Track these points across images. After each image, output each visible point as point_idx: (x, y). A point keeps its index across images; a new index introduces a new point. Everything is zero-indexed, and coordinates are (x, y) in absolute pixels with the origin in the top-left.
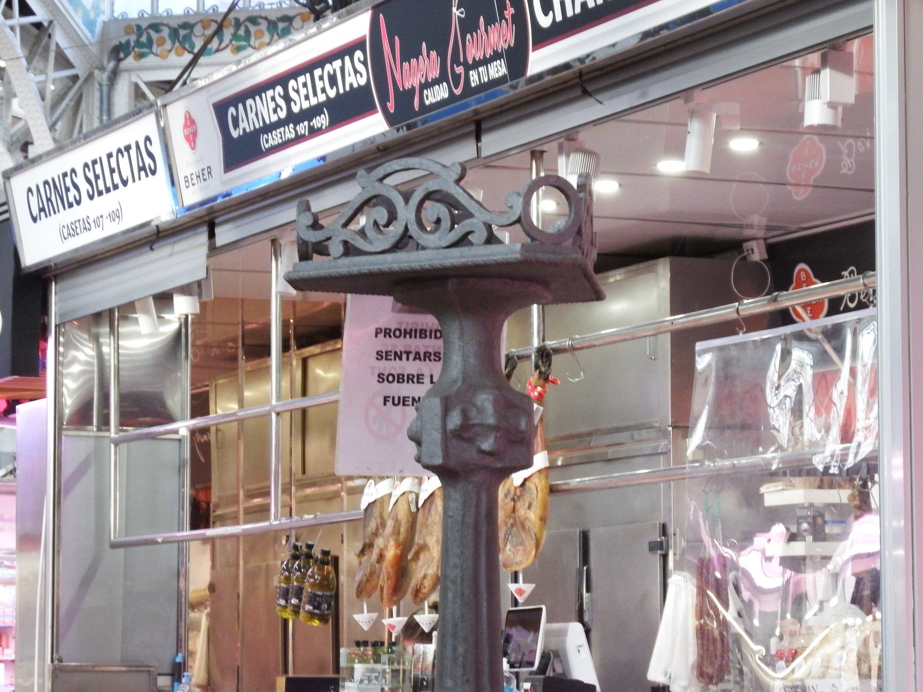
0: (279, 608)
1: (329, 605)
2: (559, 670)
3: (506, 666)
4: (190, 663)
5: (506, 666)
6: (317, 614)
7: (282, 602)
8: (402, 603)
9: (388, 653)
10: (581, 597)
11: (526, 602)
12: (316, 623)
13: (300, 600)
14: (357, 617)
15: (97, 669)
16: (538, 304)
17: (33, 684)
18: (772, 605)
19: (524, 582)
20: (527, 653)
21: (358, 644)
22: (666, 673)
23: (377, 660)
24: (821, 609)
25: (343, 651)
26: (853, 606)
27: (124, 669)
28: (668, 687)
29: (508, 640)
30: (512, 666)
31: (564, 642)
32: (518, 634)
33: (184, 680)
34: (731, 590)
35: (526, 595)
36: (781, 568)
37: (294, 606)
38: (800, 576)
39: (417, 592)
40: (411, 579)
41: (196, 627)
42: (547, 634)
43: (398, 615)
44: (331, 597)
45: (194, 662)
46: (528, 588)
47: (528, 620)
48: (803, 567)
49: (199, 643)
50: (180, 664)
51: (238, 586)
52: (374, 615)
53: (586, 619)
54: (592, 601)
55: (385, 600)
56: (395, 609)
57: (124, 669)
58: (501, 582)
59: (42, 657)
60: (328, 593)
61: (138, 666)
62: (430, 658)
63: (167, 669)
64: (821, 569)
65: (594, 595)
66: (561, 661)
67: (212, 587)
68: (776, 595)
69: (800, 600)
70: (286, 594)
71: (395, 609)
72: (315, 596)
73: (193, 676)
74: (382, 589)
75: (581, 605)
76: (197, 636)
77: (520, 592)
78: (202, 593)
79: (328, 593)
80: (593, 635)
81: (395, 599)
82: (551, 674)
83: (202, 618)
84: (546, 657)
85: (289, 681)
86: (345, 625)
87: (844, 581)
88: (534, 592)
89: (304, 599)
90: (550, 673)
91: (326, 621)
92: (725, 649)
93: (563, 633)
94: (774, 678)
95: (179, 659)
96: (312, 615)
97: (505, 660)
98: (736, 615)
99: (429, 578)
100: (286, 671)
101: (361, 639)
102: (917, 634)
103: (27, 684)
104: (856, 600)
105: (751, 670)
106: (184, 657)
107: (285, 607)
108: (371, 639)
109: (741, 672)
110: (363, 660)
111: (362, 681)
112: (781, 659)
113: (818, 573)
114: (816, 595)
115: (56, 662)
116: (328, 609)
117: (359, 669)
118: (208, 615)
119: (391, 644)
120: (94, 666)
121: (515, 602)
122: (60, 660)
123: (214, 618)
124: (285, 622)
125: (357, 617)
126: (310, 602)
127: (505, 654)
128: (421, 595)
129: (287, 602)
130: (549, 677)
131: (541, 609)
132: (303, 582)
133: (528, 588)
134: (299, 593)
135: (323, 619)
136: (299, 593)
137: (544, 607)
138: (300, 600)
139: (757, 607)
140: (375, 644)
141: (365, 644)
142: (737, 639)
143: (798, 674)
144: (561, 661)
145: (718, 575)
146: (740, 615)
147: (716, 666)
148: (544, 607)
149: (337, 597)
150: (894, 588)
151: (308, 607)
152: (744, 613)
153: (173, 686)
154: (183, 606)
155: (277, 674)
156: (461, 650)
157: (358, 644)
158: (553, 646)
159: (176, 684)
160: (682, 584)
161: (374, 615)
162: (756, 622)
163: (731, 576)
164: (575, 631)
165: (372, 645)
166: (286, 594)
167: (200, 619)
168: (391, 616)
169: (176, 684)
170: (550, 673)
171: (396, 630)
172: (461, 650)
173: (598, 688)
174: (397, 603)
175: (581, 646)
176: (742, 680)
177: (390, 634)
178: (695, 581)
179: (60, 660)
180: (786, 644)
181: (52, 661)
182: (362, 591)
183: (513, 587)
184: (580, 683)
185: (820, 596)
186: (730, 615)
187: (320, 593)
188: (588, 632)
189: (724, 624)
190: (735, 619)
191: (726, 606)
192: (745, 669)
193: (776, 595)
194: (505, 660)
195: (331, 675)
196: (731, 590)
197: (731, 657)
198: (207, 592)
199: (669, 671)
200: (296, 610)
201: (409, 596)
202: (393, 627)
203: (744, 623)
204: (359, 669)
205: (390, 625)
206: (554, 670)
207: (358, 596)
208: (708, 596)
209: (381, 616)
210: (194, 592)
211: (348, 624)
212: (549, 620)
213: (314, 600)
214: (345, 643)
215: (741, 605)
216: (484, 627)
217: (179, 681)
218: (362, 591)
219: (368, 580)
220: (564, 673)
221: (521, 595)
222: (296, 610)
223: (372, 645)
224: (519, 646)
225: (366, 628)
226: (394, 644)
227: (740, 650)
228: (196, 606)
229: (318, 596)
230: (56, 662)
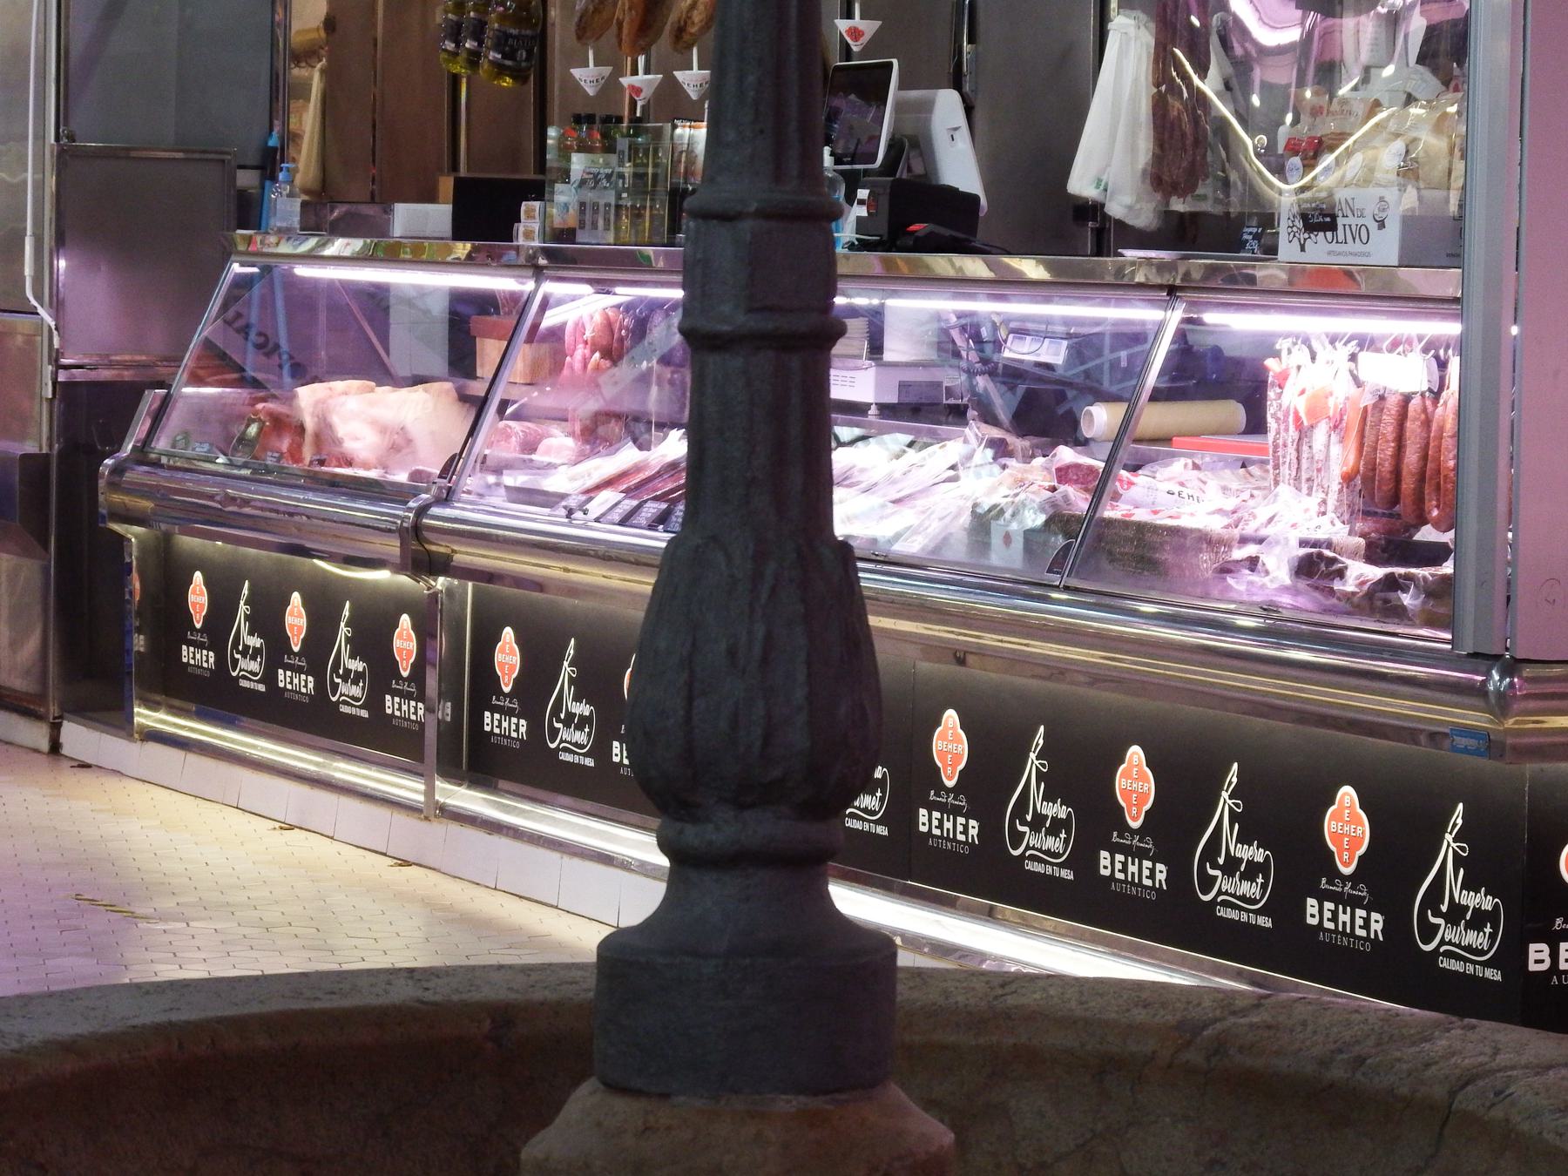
0: (443, 56)
1: (530, 52)
2: (918, 169)
3: (828, 160)
4: (292, 152)
5: (828, 160)
6: (509, 67)
7: (450, 46)
8: (654, 48)
9: (629, 135)
10: (959, 51)
11: (865, 53)
12: (507, 82)
13: (481, 44)
14: (577, 73)
15: (133, 154)
16: (832, 292)
17: (25, 182)
18: (1282, 74)
19: (862, 18)
20: (864, 140)
21: (578, 120)
22: (1099, 181)
23: (609, 148)
24: (1366, 80)
25: (552, 132)
26: (1420, 67)
27: (180, 155)
28: (1103, 205)
29: (833, 116)
30: (838, 160)
31: (928, 121)
32: (849, 105)
33: (281, 176)
34: (1214, 41)
35: (865, 39)
36: (1299, 13)
37: (470, 52)
38: (1330, 21)
39: (680, 31)
40: (669, 9)
41: (303, 91)
42: (900, 107)
43: (647, 72)
44: (533, 38)
45: (299, 152)
46: (869, 27)
47: (871, 84)
48: (1338, 8)
49: (307, 120)
50: (274, 149)
51: (375, 25)
52: (607, 70)
53: (967, 88)
54: (976, 57)
55: (625, 45)
56: (641, 60)
57: (180, 155)
58: (824, 16)
59: (40, 136)
60: (528, 32)
61: (204, 152)
62: (700, 148)
63: (253, 157)
64: (1368, 11)
65: (980, 48)
66: (921, 154)
67: (330, 24)
68: (1289, 58)
69: (1328, 72)
70: (455, 33)
71: (641, 60)
72: (507, 36)
73: (296, 170)
74: (620, 25)
75: (959, 65)
76: (305, 108)
77: (856, 33)
78: (314, 35)
79: (528, 32)
80: (978, 114)
81: (642, 43)
82: (905, 176)
83: (314, 78)
84: (895, 146)
85: (459, 183)
86: (557, 92)
87: (1406, 36)
88: (877, 35)
89: (488, 42)
90: (902, 173)
91: (525, 80)
92: (1199, 142)
93: (927, 107)
94: (1280, 193)
95: (273, 142)
96: (500, 70)
97: (827, 150)
98: (1221, 87)
99: (701, 7)
100: (455, 167)
101: (583, 111)
102: (1527, 117)
103: (15, 181)
104: (1426, 57)
105: (1244, 178)
106: (282, 138)
107: (455, 54)
108: (600, 113)
109: (1226, 184)
110: (583, 148)
111: (583, 183)
112: (1296, 154)
113: (1363, 18)
114: (1357, 59)
115: (64, 141)
116: (527, 59)
117: (579, 164)
118: (322, 71)
119: (634, 120)
120: (128, 149)
121: (847, 53)
122: (71, 138)
123: (332, 77)
124: (455, 80)
125: (577, 73)
126: (497, 47)
127: (828, 142)
128: (686, 37)
129: (458, 46)
130: (900, 180)
131: (891, 64)
132: (487, 13)
133: (869, 27)
134: (478, 32)
135: (519, 76)
136: (478, 32)
137: (895, 62)
138: (481, 44)
139: (1257, 74)
140: (607, 120)
141: (590, 119)
142: (1222, 126)
143: (1326, 182)
144: (921, 154)
145: (1195, 21)
146: (1228, 86)
147: (1185, 164)
148: (895, 62)
149: (542, 38)
150: (1492, 52)
151: (493, 55)
152: (1234, 83)
153: (263, 188)
154: (282, 54)
155: (440, 170)
156: (751, 79)
157: (578, 120)
158: (909, 129)
159: (268, 183)
160: (1132, 31)
161: (607, 70)
162: (1256, 100)
163: (1215, 20)
164: (947, 104)
165: (601, 124)
166: (455, 33)
167: (311, 78)
168: (635, 72)
169: (268, 183)
170: (902, 173)
171: (643, 95)
172: (751, 79)
173: (983, 201)
174: (645, 50)
175: (956, 129)
176: (1228, 196)
177: (633, 104)
178: (1152, 26)
179: (71, 138)
180: (1304, 129)
181: (57, 139)
182: (586, 29)
183: (843, 25)
184: (953, 192)
185: (1365, 57)
186: (1209, 87)
187: (514, 32)
188: (969, 110)
189: (1200, 99)
190: (1218, 94)
191: (1203, 71)
192: (1234, 176)
193: (1289, 58)
194: (827, 150)
195: (530, 175)
196: (1214, 41)
197: (1209, 159)
198: (323, 34)
199: (1104, 178)
200: (474, 59)
201: (664, 42)
202: (638, 91)
203: (1235, 101)
204: (579, 164)
205: (632, 87)
206: (909, 169)
207: (579, 38)
208: (1174, 56)
209: (618, 72)
210: (298, 32)
211: (561, 89)
212: (903, 86)
213: (501, 42)
214: (556, 118)
215: (1230, 70)
216: (793, 40)
217: (274, 179)
218: (586, 29)
219: (596, 10)
220: (925, 175)
221: (856, 39)
222: (474, 59)
223: (601, 124)
224: (851, 128)
225: (591, 92)
226: (639, 120)
227: (1226, 148)
228: (304, 56)
229: (511, 36)
230: (64, 141)
